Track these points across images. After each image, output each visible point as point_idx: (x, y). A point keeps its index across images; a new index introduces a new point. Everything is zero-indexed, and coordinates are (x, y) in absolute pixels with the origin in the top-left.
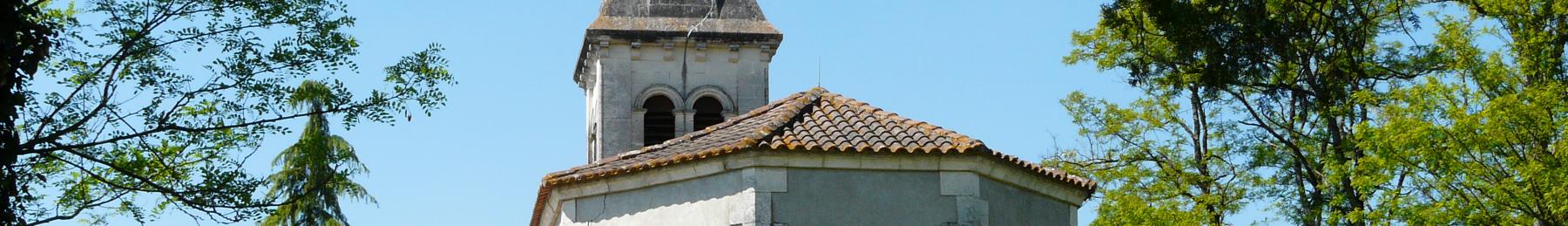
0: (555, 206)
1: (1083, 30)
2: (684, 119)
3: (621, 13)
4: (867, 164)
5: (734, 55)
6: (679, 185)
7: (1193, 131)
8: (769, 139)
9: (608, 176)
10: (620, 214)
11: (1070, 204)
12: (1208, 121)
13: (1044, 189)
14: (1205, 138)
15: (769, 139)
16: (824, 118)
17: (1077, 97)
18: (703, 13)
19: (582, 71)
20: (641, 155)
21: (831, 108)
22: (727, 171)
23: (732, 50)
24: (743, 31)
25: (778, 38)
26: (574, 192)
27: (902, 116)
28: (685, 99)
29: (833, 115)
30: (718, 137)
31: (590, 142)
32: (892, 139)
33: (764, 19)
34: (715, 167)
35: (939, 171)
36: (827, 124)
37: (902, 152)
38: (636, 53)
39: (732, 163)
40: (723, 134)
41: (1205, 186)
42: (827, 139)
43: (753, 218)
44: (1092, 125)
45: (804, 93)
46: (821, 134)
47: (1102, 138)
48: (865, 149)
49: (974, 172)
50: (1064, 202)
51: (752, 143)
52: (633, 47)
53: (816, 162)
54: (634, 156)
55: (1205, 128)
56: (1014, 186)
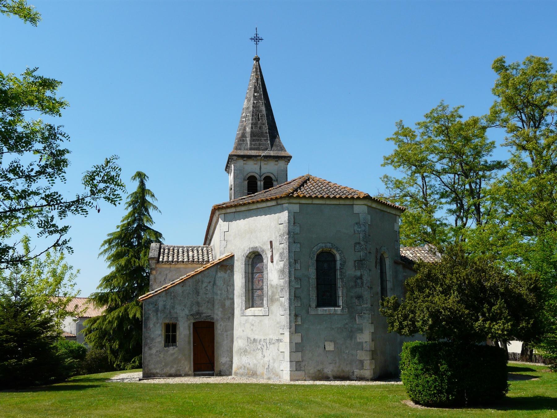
0: (217, 216)
1: (387, 156)
2: (260, 184)
3: (240, 149)
4: (328, 202)
5: (277, 163)
6: (261, 209)
7: (422, 187)
8: (293, 193)
9: (236, 206)
10: (240, 219)
11: (396, 215)
12: (427, 184)
13: (389, 210)
14: (426, 189)
15: (293, 193)
16: (311, 185)
17: (386, 177)
18: (266, 149)
19: (227, 168)
20: (247, 199)
21: (313, 182)
22: (278, 204)
23: (276, 161)
24: (279, 155)
25: (291, 157)
26: (224, 211)
27: (339, 184)
28: (260, 177)
29: (314, 184)
30: (273, 192)
31: (230, 190)
32: (336, 193)
33: (286, 151)
34: (273, 203)
35: (353, 204)
36: (313, 187)
37: (340, 198)
38: (245, 162)
39: (279, 202)
40: (276, 191)
41: (426, 205)
42: (313, 193)
43: (287, 221)
44: (391, 186)
45: (303, 176)
46: (311, 191)
47: (394, 190)
48: (327, 197)
49: (365, 205)
50: (395, 215)
51: (286, 195)
52: (244, 160)
53: (309, 201)
54: (245, 198)
55: (426, 187)
56: (379, 209)
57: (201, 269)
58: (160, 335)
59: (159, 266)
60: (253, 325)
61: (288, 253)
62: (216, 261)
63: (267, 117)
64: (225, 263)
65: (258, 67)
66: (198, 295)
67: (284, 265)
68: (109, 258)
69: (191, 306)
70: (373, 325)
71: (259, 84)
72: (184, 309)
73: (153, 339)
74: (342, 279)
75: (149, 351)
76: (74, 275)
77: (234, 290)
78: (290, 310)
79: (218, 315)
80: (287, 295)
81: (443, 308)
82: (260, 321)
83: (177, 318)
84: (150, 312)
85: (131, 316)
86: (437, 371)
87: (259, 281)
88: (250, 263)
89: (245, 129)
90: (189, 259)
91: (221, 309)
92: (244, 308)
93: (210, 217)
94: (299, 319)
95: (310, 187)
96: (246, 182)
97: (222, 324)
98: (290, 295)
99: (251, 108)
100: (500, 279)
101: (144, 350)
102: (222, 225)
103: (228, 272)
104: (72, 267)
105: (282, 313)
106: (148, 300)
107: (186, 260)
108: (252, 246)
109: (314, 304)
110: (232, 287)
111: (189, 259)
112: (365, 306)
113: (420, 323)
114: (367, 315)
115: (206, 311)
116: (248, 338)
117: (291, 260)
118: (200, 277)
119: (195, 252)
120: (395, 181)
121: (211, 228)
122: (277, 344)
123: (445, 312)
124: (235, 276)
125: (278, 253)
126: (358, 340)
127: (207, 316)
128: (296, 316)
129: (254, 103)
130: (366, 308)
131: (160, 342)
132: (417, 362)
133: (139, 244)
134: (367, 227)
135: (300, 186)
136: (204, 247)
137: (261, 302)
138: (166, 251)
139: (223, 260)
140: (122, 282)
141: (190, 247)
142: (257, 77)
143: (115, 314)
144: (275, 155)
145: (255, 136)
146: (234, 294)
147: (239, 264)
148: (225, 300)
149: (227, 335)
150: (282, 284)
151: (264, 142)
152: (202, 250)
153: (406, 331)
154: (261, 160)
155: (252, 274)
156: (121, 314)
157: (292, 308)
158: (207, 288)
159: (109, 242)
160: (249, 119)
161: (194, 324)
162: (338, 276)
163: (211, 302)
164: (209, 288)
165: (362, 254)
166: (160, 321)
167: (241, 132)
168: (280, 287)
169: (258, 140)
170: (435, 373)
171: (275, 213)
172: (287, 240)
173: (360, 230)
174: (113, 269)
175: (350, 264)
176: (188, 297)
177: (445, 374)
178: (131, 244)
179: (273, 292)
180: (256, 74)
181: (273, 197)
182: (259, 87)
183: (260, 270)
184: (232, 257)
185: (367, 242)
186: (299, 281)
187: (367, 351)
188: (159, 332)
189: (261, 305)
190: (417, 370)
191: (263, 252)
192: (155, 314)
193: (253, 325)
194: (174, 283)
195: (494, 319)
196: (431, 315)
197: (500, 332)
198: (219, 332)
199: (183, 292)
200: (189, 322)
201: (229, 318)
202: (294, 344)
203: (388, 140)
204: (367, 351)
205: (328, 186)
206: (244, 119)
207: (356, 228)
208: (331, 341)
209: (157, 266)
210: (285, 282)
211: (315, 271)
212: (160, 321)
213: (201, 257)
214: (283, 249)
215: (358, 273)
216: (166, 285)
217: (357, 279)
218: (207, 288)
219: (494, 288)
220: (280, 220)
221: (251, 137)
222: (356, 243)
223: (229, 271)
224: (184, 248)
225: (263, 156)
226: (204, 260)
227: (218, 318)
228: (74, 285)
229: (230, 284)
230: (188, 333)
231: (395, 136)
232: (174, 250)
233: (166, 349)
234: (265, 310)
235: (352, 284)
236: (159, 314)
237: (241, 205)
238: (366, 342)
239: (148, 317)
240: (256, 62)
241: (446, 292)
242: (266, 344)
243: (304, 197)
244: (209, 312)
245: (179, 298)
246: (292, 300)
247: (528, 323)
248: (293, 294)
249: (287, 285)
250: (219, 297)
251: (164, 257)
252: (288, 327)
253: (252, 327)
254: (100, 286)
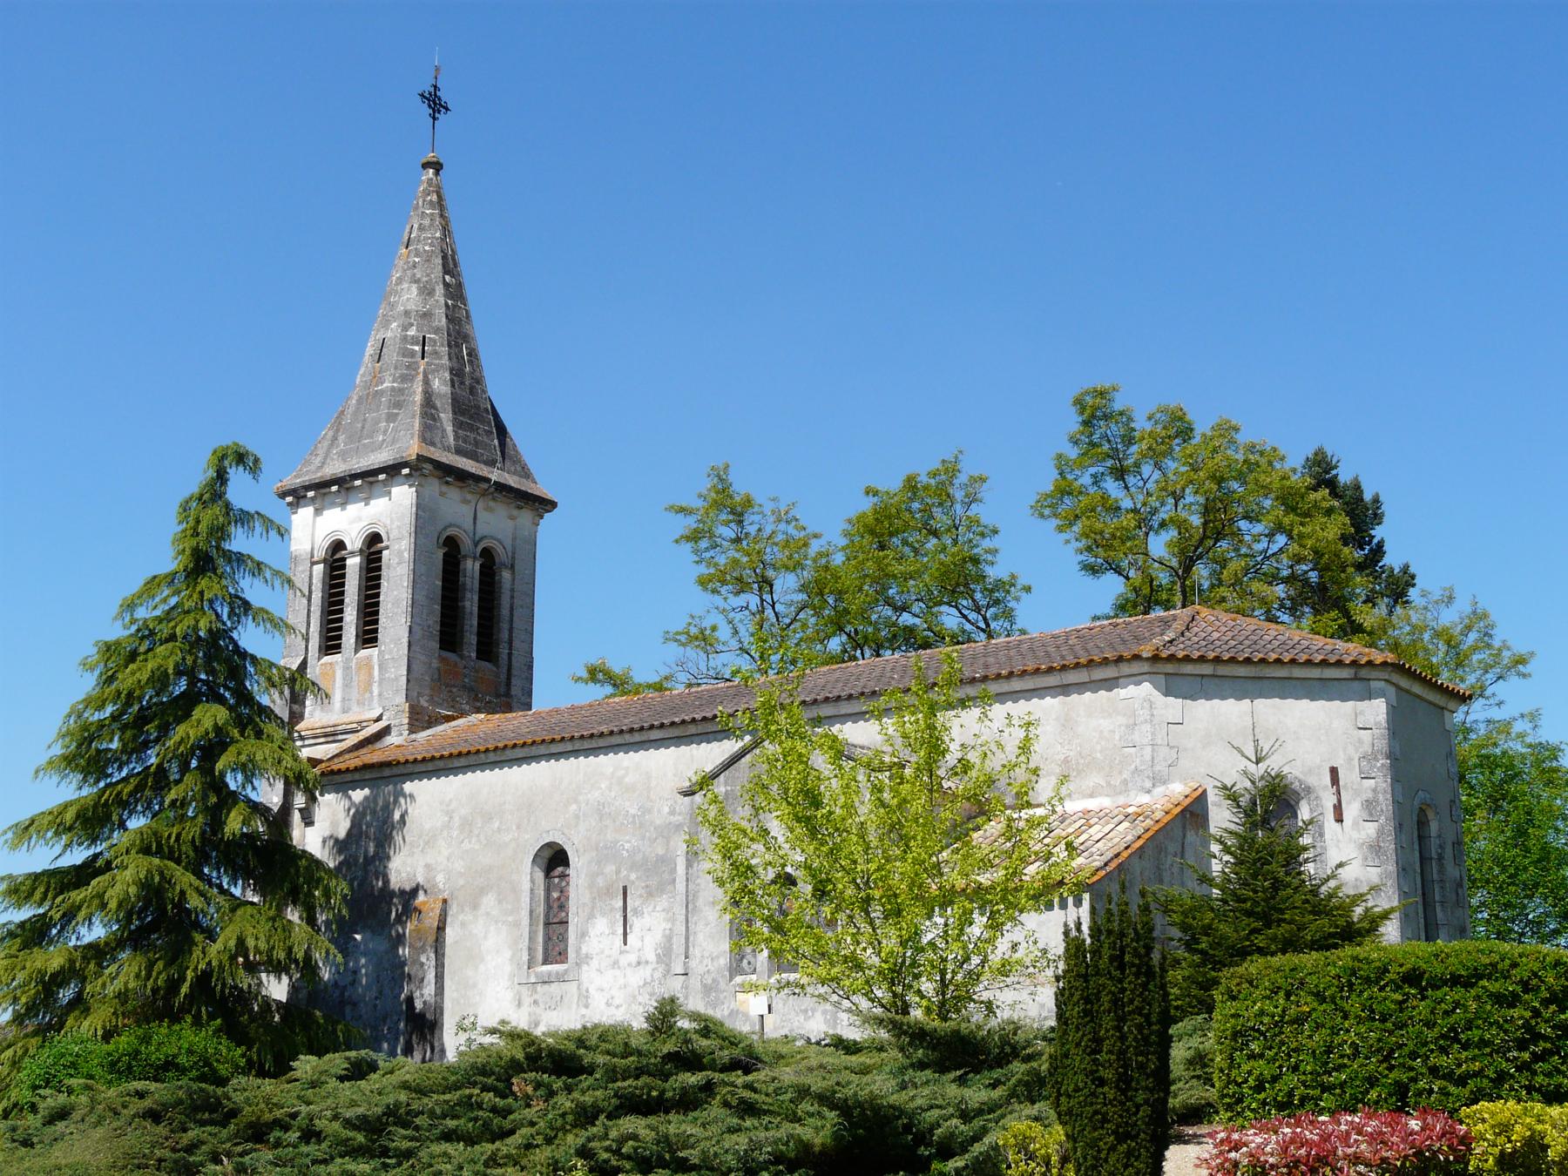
5: (515, 512)
10: (1223, 698)
22: (1356, 678)
34: (1345, 673)
38: (444, 488)
39: (1364, 673)
67: (1380, 832)
125: (1359, 800)
154: (484, 494)
171: (1344, 700)
174: (408, 787)
214: (1374, 790)
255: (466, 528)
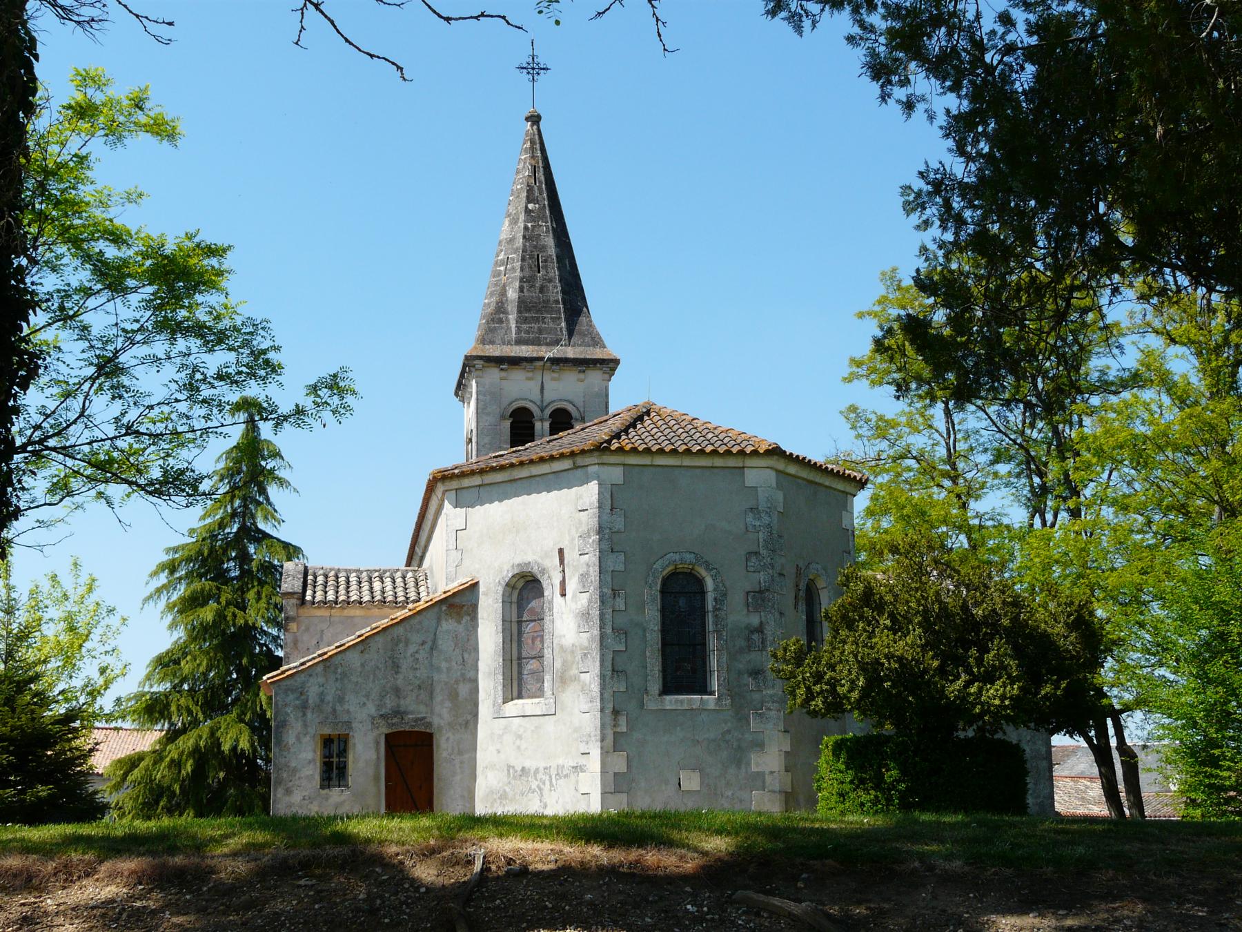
0: (440, 495)
2: (542, 426)
3: (492, 342)
4: (687, 461)
5: (582, 376)
6: (537, 479)
8: (609, 442)
9: (482, 472)
10: (491, 502)
11: (847, 493)
12: (957, 428)
13: (827, 481)
14: (955, 441)
15: (609, 442)
16: (653, 426)
17: (853, 409)
18: (556, 342)
19: (461, 388)
20: (508, 455)
21: (658, 418)
22: (576, 467)
23: (580, 371)
25: (616, 362)
26: (455, 484)
28: (542, 411)
29: (660, 423)
30: (568, 440)
31: (468, 444)
33: (605, 347)
34: (567, 464)
35: (743, 467)
37: (715, 452)
38: (503, 374)
39: (580, 461)
41: (954, 480)
43: (597, 505)
44: (864, 431)
46: (651, 438)
48: (686, 450)
49: (771, 468)
50: (843, 492)
52: (502, 369)
53: (646, 460)
54: (502, 455)
55: (955, 433)
57: (401, 614)
58: (310, 762)
59: (304, 612)
60: (520, 737)
61: (597, 573)
62: (439, 595)
63: (558, 262)
64: (457, 600)
65: (537, 137)
66: (397, 673)
67: (590, 602)
68: (170, 607)
69: (382, 697)
70: (788, 736)
71: (540, 182)
72: (364, 704)
73: (295, 770)
74: (718, 632)
75: (287, 798)
76: (114, 629)
77: (478, 660)
78: (602, 699)
79: (441, 716)
80: (595, 668)
81: (887, 657)
82: (536, 727)
83: (348, 724)
84: (289, 710)
85: (226, 747)
86: (878, 783)
87: (534, 639)
88: (515, 598)
89: (503, 293)
90: (373, 598)
91: (448, 704)
92: (500, 701)
93: (417, 523)
94: (623, 720)
95: (649, 429)
96: (507, 424)
97: (452, 737)
98: (602, 666)
99: (519, 242)
100: (1004, 602)
101: (275, 795)
102: (451, 516)
103: (464, 621)
104: (114, 609)
105: (585, 707)
106: (284, 683)
107: (366, 598)
108: (518, 560)
109: (655, 686)
110: (473, 654)
111: (373, 598)
112: (770, 692)
113: (845, 689)
114: (773, 713)
115: (414, 707)
116: (509, 767)
117: (605, 590)
118: (400, 630)
119: (388, 581)
120: (874, 419)
121: (423, 526)
122: (573, 777)
123: (890, 664)
124: (480, 630)
126: (754, 769)
127: (416, 720)
128: (616, 712)
129: (526, 228)
130: (771, 696)
131: (312, 777)
132: (843, 767)
133: (244, 573)
134: (775, 518)
135: (628, 427)
136: (407, 571)
137: (539, 685)
138: (320, 579)
139: (454, 593)
140: (205, 663)
141: (376, 571)
142: (533, 162)
143: (187, 742)
144: (578, 356)
145: (528, 310)
146: (477, 671)
147: (490, 601)
148: (457, 682)
149: (462, 762)
150: (586, 643)
151: (551, 325)
152: (404, 577)
153: (818, 703)
155: (520, 623)
156: (202, 743)
157: (606, 696)
158: (417, 656)
159: (172, 567)
160: (513, 268)
161: (388, 736)
162: (710, 626)
163: (427, 688)
164: (422, 655)
165: (762, 576)
166: (311, 731)
167: (494, 299)
168: (581, 649)
169: (537, 320)
170: (876, 788)
172: (596, 546)
173: (758, 523)
175: (737, 599)
176: (374, 674)
177: (894, 788)
178: (221, 577)
179: (564, 663)
180: (533, 157)
181: (566, 451)
182: (540, 188)
183: (538, 614)
184: (475, 586)
185: (774, 551)
186: (623, 636)
187: (774, 792)
188: (310, 755)
189: (540, 693)
190: (842, 783)
191: (544, 574)
192: (301, 714)
193: (520, 737)
194: (344, 645)
195: (989, 677)
196: (863, 667)
197: (997, 702)
198: (444, 754)
199: (363, 665)
200: (376, 732)
201: (467, 723)
202: (611, 777)
203: (861, 315)
204: (774, 792)
205: (691, 427)
206: (502, 268)
207: (750, 519)
208: (694, 769)
209: (301, 611)
210: (592, 639)
211: (658, 615)
212: (311, 731)
213: (400, 593)
214: (588, 565)
215: (755, 620)
216: (326, 650)
217: (752, 632)
218: (417, 656)
219: (992, 619)
220: (580, 502)
221: (519, 312)
222: (750, 553)
223: (466, 619)
224: (362, 572)
225: (549, 359)
226: (407, 598)
227: (442, 723)
228: (113, 650)
229: (469, 647)
230: (374, 757)
231: (877, 308)
232: (337, 577)
233: (326, 791)
234: (547, 702)
235: (741, 643)
236: (309, 715)
237: (493, 469)
238: (772, 773)
239: (285, 721)
240: (532, 126)
241: (898, 626)
242: (550, 777)
243: (634, 450)
244: (422, 711)
245: (354, 679)
246: (608, 678)
247: (1057, 688)
248: (609, 664)
249: (595, 645)
250: (444, 677)
251: (315, 592)
252: (599, 737)
253: (518, 742)
254: (148, 678)
255: (545, 398)
